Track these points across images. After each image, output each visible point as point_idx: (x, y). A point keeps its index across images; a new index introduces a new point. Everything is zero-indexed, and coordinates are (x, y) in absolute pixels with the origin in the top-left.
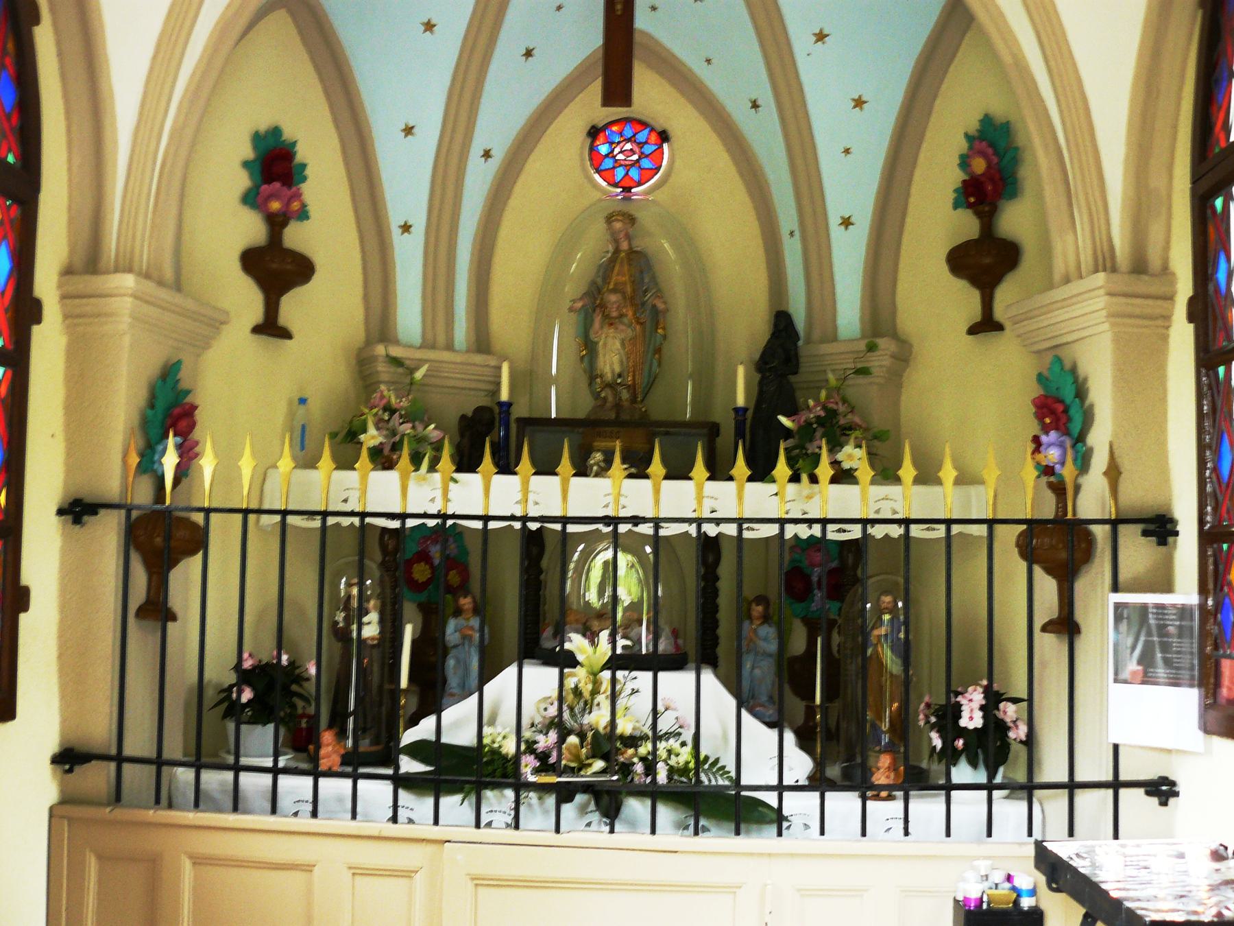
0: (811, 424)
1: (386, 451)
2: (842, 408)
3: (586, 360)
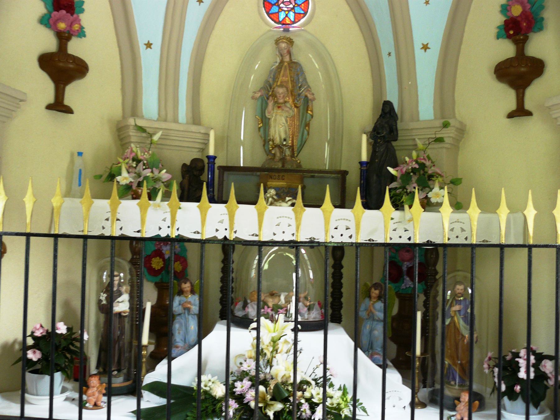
0: (409, 173)
1: (134, 187)
2: (428, 163)
3: (262, 130)
